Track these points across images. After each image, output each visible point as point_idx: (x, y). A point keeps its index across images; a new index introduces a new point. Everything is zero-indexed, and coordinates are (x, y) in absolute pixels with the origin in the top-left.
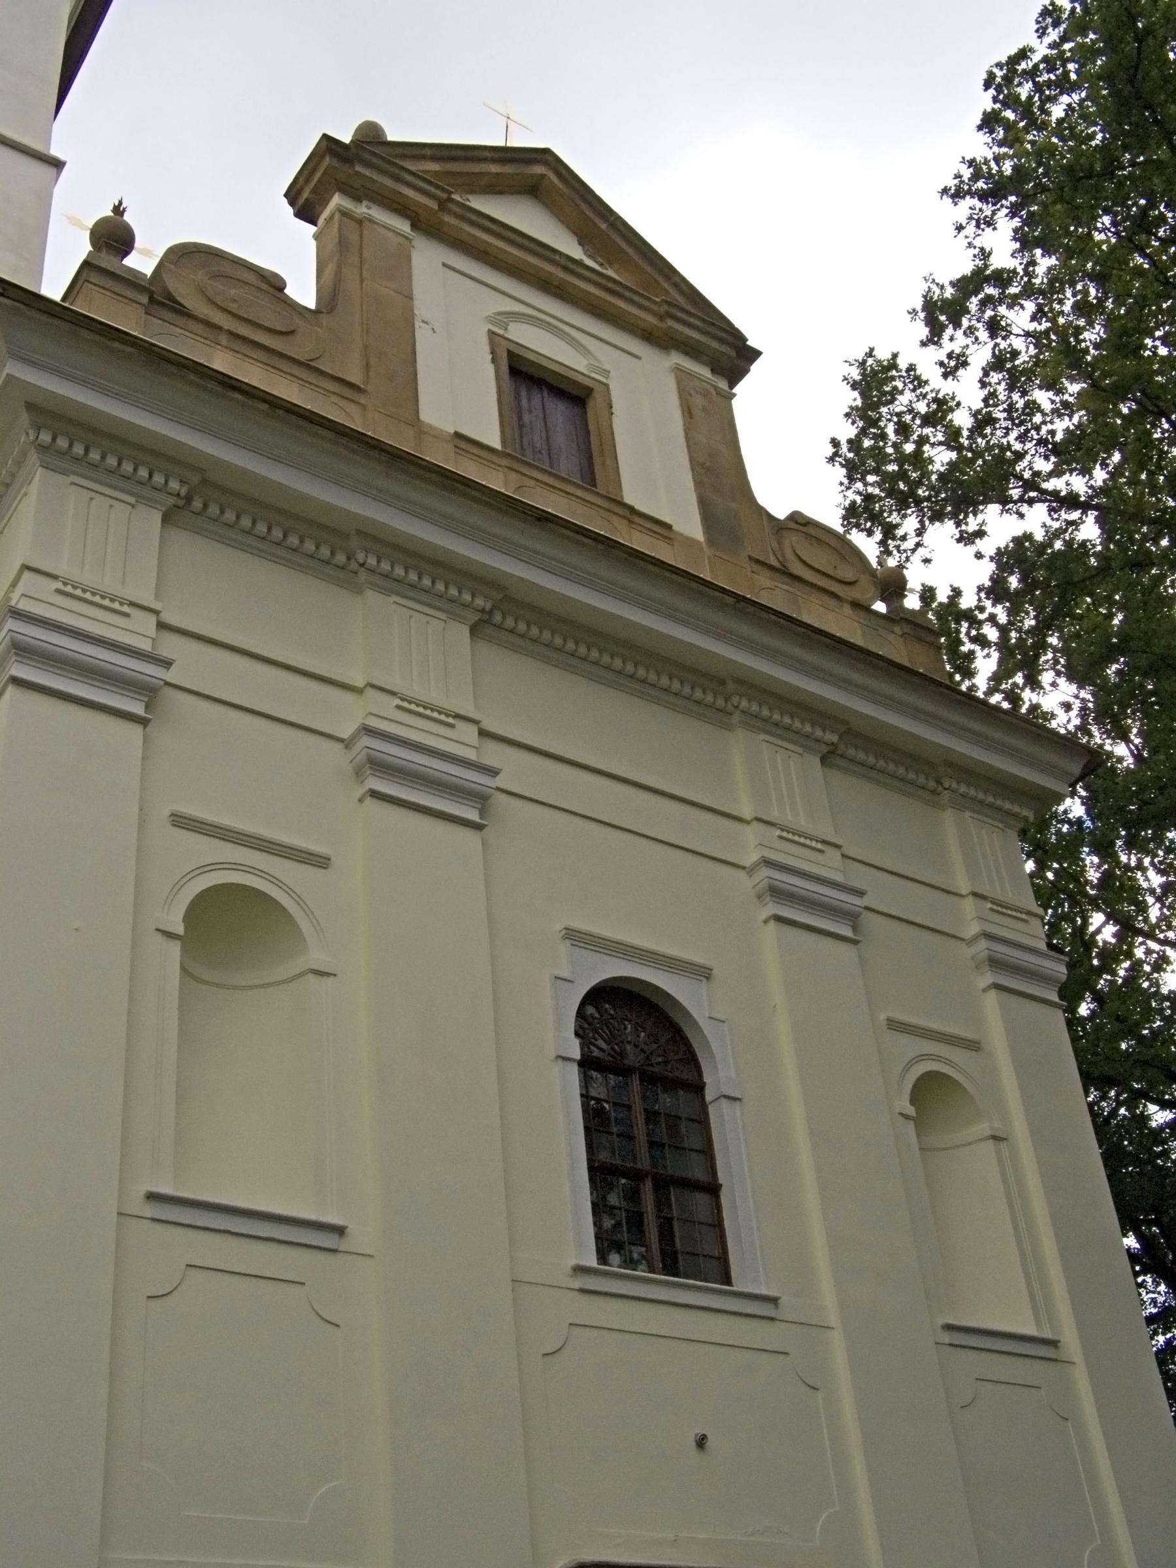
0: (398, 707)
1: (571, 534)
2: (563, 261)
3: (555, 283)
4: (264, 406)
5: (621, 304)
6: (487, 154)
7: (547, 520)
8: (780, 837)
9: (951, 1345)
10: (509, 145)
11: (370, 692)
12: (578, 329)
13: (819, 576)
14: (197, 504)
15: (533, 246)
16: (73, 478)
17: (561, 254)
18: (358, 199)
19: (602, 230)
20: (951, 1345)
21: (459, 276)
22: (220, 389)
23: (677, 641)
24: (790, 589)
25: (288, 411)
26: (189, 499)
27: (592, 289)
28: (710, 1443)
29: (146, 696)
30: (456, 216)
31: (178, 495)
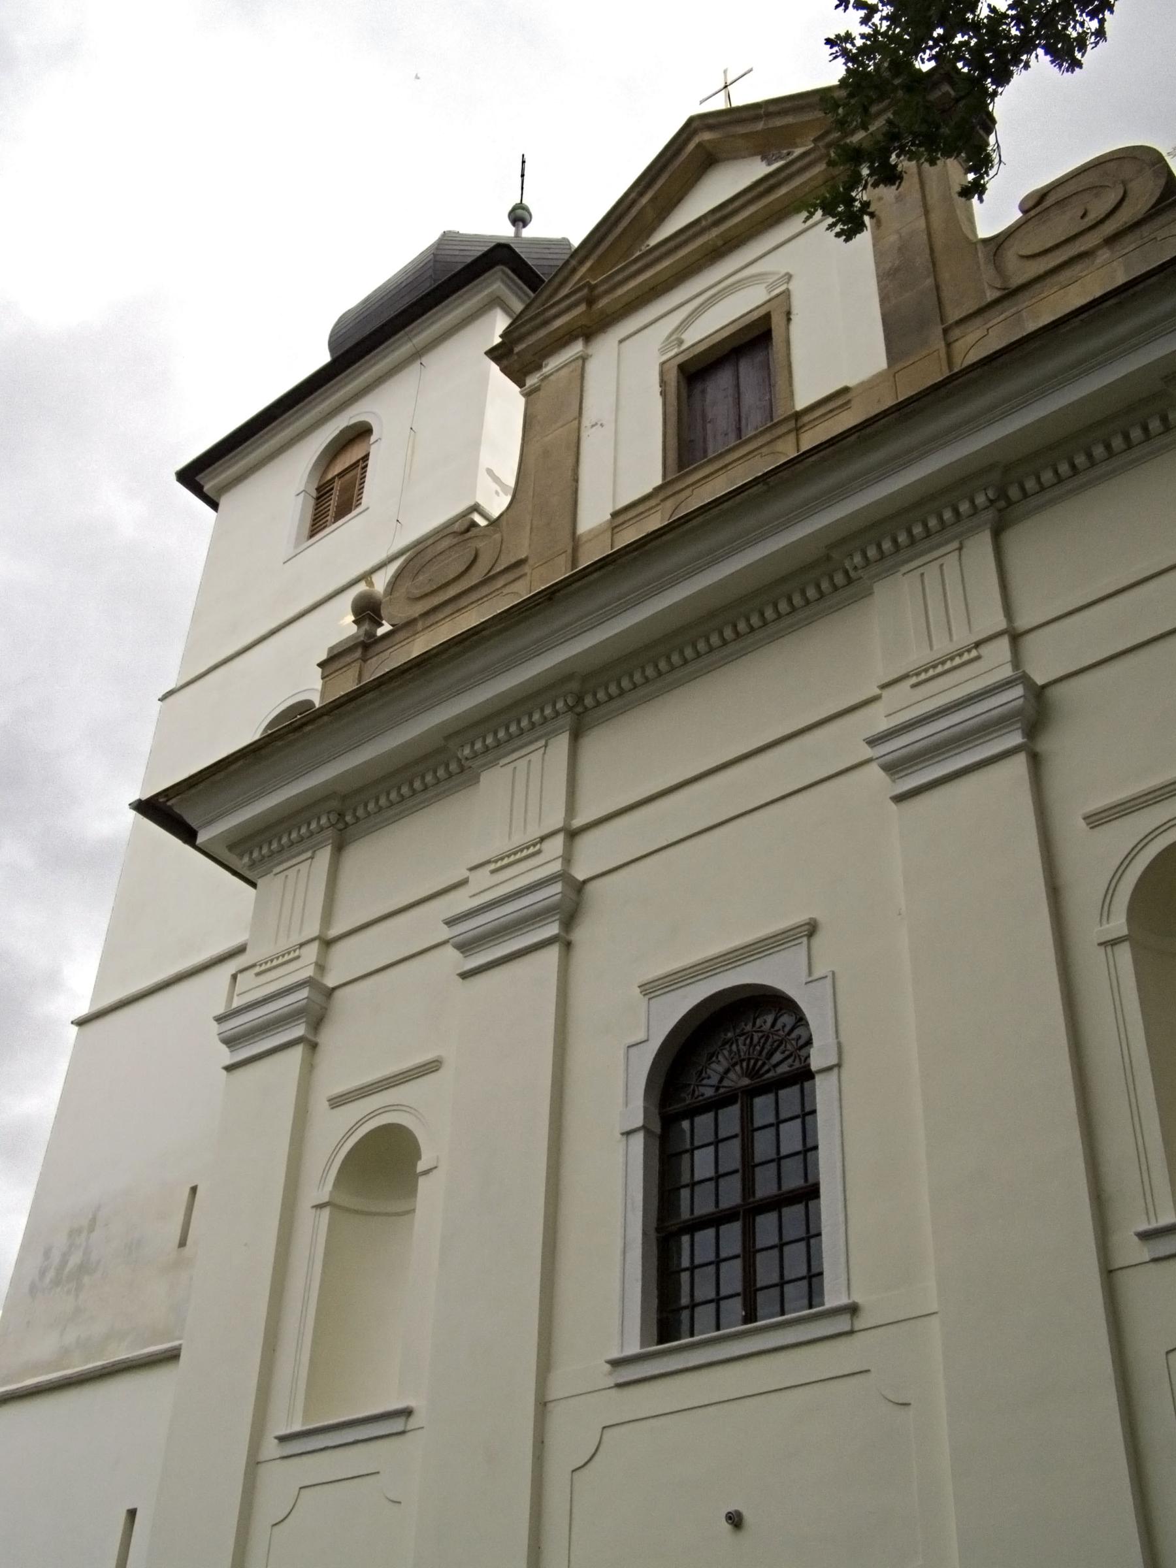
0: (493, 872)
1: (579, 584)
2: (710, 220)
3: (720, 243)
4: (326, 718)
5: (783, 190)
6: (633, 195)
7: (554, 593)
8: (914, 686)
9: (1155, 1260)
10: (734, 105)
11: (886, 693)
12: (720, 282)
13: (1057, 253)
14: (1014, 492)
15: (683, 237)
16: (503, 762)
17: (704, 217)
18: (539, 367)
19: (763, 131)
20: (1155, 1260)
21: (773, 254)
22: (297, 734)
23: (1082, 401)
24: (1003, 317)
25: (338, 707)
26: (1002, 493)
27: (666, 263)
28: (726, 1526)
29: (1016, 722)
30: (607, 292)
31: (991, 502)
